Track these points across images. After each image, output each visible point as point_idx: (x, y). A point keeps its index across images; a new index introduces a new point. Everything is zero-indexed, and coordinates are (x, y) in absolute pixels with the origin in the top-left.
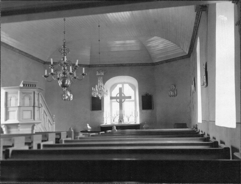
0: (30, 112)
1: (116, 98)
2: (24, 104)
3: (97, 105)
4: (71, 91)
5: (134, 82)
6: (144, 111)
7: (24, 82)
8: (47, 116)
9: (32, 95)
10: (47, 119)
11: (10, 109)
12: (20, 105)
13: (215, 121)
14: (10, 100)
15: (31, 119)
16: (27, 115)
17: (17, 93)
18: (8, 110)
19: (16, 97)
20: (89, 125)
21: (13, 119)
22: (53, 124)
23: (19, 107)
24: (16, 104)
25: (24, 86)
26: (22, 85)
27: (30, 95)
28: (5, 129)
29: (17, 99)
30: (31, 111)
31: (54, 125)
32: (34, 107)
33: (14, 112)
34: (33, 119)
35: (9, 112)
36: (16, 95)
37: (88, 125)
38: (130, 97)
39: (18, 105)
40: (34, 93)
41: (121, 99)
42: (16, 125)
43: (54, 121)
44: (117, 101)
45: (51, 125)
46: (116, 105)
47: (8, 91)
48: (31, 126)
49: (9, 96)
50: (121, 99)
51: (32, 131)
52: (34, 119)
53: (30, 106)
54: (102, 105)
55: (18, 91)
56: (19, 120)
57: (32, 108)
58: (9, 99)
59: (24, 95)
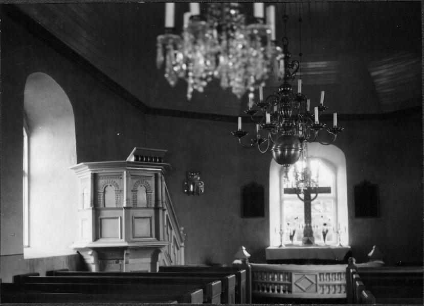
0: (148, 221)
1: (296, 191)
2: (135, 202)
3: (255, 203)
4: (200, 173)
5: (337, 155)
6: (360, 220)
7: (137, 149)
8: (171, 229)
9: (152, 183)
10: (172, 237)
11: (105, 214)
12: (129, 206)
13: (23, 254)
14: (105, 192)
15: (151, 236)
16: (143, 228)
17: (120, 176)
18: (99, 215)
19: (117, 186)
20: (246, 250)
21: (114, 238)
22: (181, 247)
23: (126, 208)
24: (118, 202)
25: (137, 159)
26: (132, 158)
27: (148, 181)
28: (95, 261)
29: (121, 191)
30: (150, 218)
31: (182, 249)
32: (157, 209)
33: (116, 220)
34: (154, 238)
35: (101, 219)
36: (117, 181)
37: (244, 248)
38: (327, 190)
39: (125, 205)
40: (156, 176)
41: (309, 194)
42: (119, 251)
43: (182, 242)
44: (298, 196)
45: (178, 249)
46: (295, 206)
47: (101, 171)
48: (152, 252)
49: (101, 182)
50: (309, 194)
51: (153, 264)
52: (157, 237)
53: (147, 208)
54: (354, 204)
55: (123, 172)
56: (127, 240)
57: (151, 213)
58: (101, 191)
59: (135, 181)
